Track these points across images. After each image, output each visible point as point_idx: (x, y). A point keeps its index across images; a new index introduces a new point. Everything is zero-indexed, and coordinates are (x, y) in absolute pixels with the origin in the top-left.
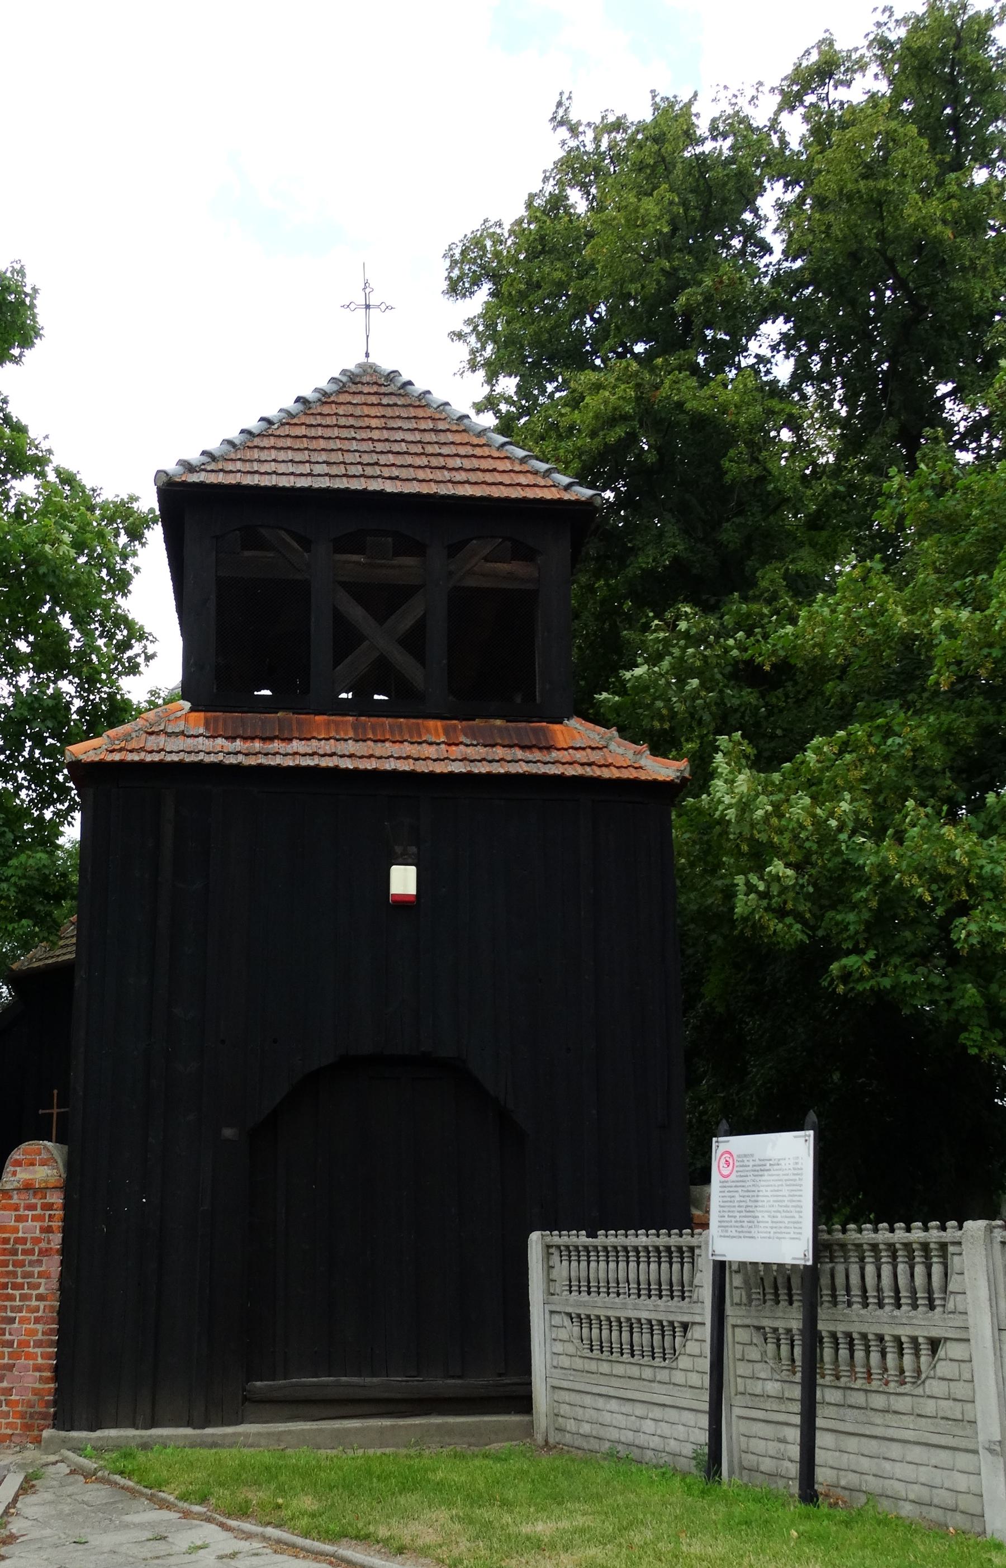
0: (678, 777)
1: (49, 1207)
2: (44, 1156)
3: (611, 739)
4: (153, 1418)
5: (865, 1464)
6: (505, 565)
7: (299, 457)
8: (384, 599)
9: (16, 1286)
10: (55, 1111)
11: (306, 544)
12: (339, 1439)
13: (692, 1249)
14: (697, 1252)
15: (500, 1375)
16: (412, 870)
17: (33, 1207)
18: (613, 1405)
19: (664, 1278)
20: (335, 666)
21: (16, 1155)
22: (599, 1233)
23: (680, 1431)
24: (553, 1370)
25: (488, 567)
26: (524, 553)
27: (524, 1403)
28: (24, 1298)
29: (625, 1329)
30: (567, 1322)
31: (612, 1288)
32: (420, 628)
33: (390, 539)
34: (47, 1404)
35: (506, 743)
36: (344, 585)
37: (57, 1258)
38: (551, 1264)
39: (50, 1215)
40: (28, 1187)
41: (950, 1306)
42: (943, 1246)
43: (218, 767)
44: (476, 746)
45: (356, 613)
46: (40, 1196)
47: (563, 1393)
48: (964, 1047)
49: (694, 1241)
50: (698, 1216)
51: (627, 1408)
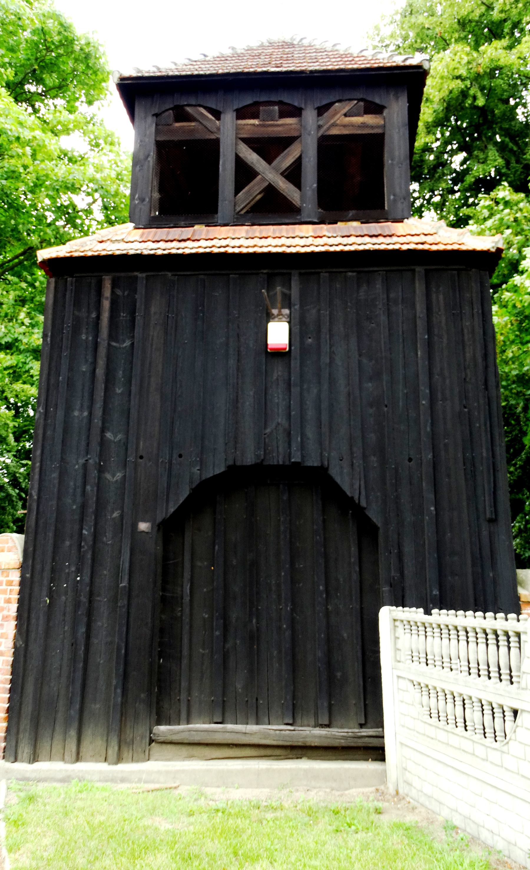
0: (493, 247)
2: (10, 544)
3: (439, 227)
4: (78, 753)
11: (217, 114)
14: (523, 637)
15: (361, 726)
25: (346, 119)
27: (376, 752)
31: (447, 663)
32: (298, 163)
33: (276, 108)
35: (358, 234)
36: (245, 141)
38: (397, 635)
43: (139, 257)
45: (252, 158)
46: (5, 574)
49: (519, 627)
50: (525, 596)
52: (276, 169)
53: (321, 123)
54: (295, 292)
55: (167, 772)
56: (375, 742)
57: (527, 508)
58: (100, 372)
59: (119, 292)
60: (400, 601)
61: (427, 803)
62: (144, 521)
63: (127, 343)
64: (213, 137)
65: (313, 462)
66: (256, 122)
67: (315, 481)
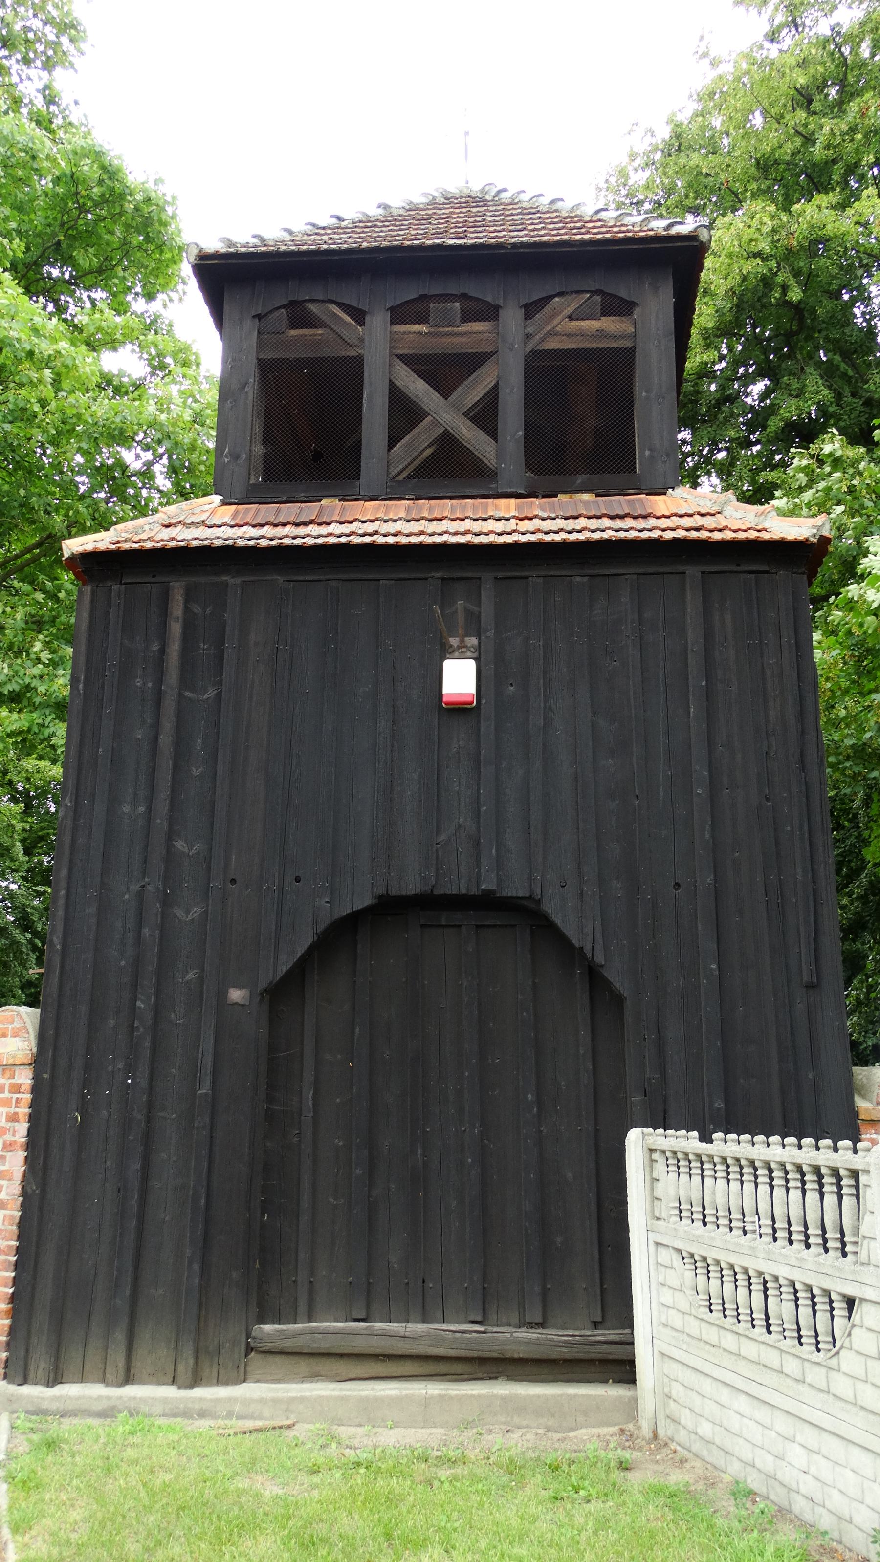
0: (814, 536)
2: (17, 1024)
6: (593, 322)
11: (359, 316)
13: (855, 1174)
14: (863, 1179)
15: (596, 1325)
18: (742, 1404)
19: (813, 1217)
20: (391, 446)
22: (715, 1136)
24: (661, 1328)
25: (573, 324)
26: (620, 307)
27: (621, 1368)
29: (757, 1287)
30: (677, 1261)
31: (737, 1221)
32: (492, 397)
33: (457, 305)
36: (403, 358)
37: (22, 1155)
38: (654, 1176)
39: (17, 1099)
44: (554, 519)
46: (8, 1074)
47: (675, 1366)
49: (857, 1162)
50: (867, 1110)
51: (762, 1414)
53: (530, 330)
54: (487, 610)
55: (275, 1401)
56: (618, 1352)
58: (166, 740)
59: (197, 609)
60: (661, 1119)
61: (704, 1453)
62: (239, 987)
63: (211, 693)
64: (352, 353)
65: (516, 889)
66: (423, 328)
67: (524, 916)
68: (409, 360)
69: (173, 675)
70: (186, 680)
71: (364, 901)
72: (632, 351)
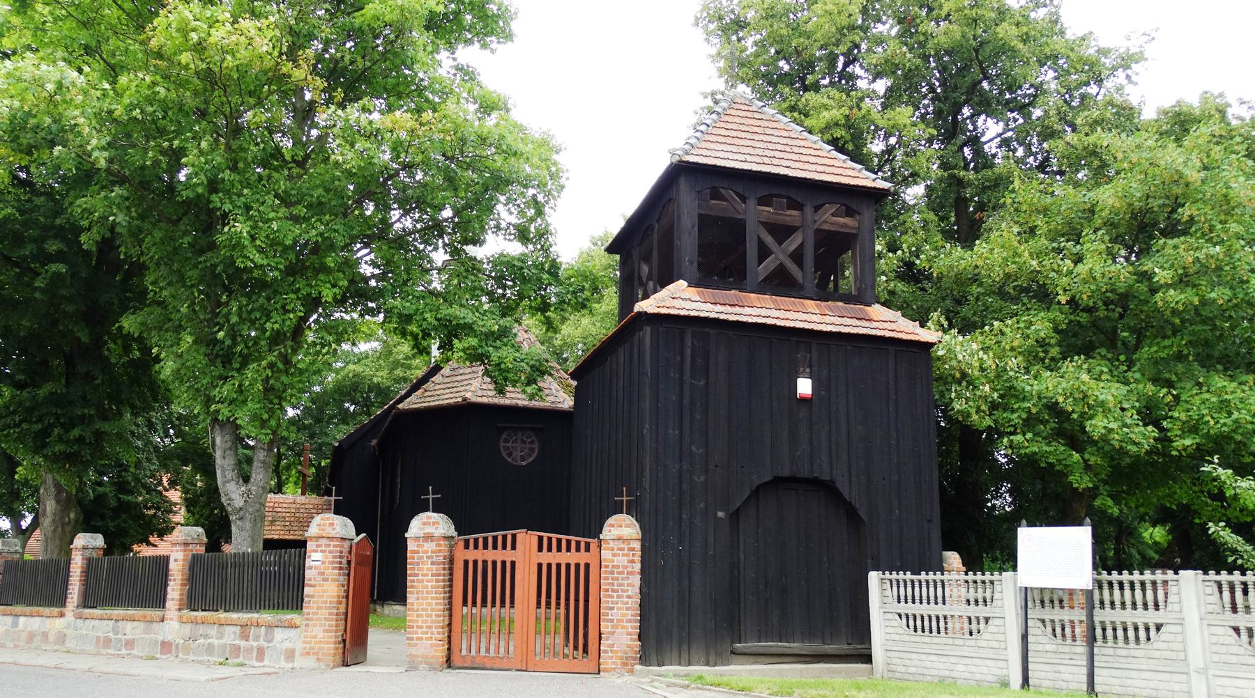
1: (633, 549)
2: (628, 522)
5: (1114, 681)
7: (734, 149)
8: (781, 232)
9: (613, 591)
10: (431, 497)
12: (752, 672)
16: (809, 382)
17: (622, 549)
18: (934, 658)
21: (611, 521)
23: (985, 670)
25: (831, 218)
26: (850, 213)
27: (867, 658)
28: (618, 597)
34: (636, 652)
40: (620, 539)
41: (1170, 607)
42: (992, 582)
48: (1071, 483)
51: (944, 659)
52: (783, 251)
56: (866, 652)
57: (252, 40)
65: (826, 477)
67: (828, 489)
68: (764, 224)
69: (687, 373)
70: (692, 377)
71: (768, 478)
72: (855, 236)
